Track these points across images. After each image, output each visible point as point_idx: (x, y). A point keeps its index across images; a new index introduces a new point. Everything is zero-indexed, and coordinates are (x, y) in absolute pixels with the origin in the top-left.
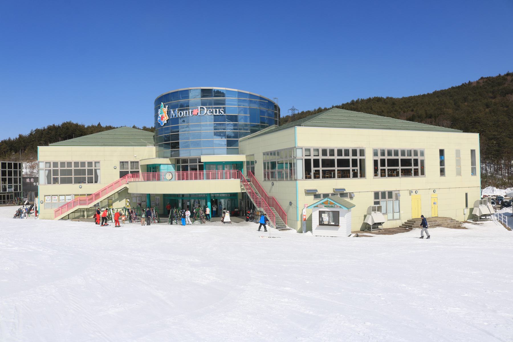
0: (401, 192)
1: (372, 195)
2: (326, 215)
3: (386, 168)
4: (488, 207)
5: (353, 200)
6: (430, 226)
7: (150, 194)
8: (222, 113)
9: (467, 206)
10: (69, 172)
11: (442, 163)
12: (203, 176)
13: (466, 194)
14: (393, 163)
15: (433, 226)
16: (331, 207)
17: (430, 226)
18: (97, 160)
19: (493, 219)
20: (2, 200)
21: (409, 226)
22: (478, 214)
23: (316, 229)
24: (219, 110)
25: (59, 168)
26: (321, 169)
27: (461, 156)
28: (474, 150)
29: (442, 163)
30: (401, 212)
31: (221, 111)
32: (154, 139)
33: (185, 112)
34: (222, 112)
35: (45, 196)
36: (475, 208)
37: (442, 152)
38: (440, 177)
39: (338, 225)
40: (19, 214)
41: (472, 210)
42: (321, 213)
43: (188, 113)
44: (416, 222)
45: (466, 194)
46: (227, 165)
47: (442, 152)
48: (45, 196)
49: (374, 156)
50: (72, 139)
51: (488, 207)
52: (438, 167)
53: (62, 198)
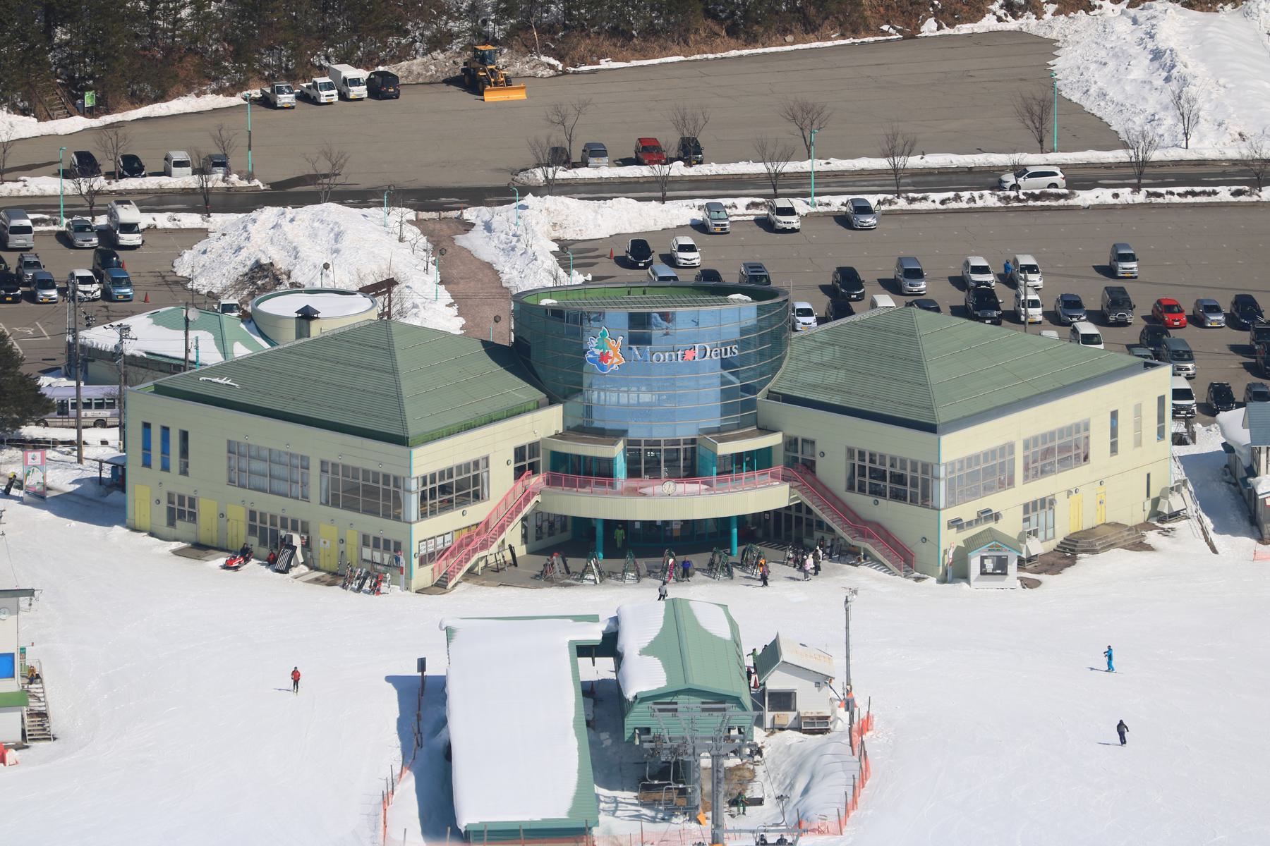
0: (1057, 498)
1: (1021, 508)
2: (990, 561)
3: (1074, 452)
4: (1182, 496)
5: (1014, 487)
6: (1102, 549)
7: (1042, 153)
8: (734, 353)
9: (1148, 495)
10: (881, 475)
11: (1114, 433)
12: (165, 450)
13: (1148, 475)
14: (444, 489)
15: (1104, 548)
16: (998, 550)
17: (1102, 549)
18: (484, 454)
19: (1191, 514)
20: (454, 495)
21: (1071, 550)
22: (1166, 511)
23: (977, 580)
24: (731, 348)
25: (867, 464)
26: (867, 480)
27: (1143, 413)
28: (1164, 396)
29: (1114, 433)
30: (1056, 527)
31: (734, 350)
32: (851, 745)
33: (667, 354)
34: (736, 351)
35: (420, 542)
36: (1162, 500)
37: (1114, 415)
38: (1111, 456)
39: (1006, 574)
40: (227, 567)
41: (1156, 502)
42: (983, 558)
43: (674, 357)
44: (1080, 541)
45: (1148, 475)
46: (21, 599)
47: (1114, 415)
48: (420, 542)
49: (249, 534)
50: (967, 537)
51: (1182, 496)
52: (1108, 441)
53: (440, 540)
